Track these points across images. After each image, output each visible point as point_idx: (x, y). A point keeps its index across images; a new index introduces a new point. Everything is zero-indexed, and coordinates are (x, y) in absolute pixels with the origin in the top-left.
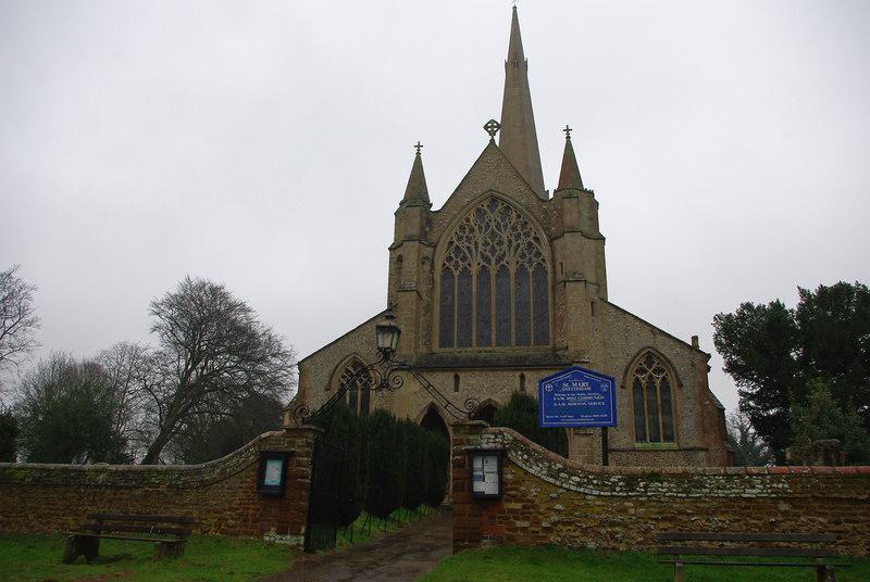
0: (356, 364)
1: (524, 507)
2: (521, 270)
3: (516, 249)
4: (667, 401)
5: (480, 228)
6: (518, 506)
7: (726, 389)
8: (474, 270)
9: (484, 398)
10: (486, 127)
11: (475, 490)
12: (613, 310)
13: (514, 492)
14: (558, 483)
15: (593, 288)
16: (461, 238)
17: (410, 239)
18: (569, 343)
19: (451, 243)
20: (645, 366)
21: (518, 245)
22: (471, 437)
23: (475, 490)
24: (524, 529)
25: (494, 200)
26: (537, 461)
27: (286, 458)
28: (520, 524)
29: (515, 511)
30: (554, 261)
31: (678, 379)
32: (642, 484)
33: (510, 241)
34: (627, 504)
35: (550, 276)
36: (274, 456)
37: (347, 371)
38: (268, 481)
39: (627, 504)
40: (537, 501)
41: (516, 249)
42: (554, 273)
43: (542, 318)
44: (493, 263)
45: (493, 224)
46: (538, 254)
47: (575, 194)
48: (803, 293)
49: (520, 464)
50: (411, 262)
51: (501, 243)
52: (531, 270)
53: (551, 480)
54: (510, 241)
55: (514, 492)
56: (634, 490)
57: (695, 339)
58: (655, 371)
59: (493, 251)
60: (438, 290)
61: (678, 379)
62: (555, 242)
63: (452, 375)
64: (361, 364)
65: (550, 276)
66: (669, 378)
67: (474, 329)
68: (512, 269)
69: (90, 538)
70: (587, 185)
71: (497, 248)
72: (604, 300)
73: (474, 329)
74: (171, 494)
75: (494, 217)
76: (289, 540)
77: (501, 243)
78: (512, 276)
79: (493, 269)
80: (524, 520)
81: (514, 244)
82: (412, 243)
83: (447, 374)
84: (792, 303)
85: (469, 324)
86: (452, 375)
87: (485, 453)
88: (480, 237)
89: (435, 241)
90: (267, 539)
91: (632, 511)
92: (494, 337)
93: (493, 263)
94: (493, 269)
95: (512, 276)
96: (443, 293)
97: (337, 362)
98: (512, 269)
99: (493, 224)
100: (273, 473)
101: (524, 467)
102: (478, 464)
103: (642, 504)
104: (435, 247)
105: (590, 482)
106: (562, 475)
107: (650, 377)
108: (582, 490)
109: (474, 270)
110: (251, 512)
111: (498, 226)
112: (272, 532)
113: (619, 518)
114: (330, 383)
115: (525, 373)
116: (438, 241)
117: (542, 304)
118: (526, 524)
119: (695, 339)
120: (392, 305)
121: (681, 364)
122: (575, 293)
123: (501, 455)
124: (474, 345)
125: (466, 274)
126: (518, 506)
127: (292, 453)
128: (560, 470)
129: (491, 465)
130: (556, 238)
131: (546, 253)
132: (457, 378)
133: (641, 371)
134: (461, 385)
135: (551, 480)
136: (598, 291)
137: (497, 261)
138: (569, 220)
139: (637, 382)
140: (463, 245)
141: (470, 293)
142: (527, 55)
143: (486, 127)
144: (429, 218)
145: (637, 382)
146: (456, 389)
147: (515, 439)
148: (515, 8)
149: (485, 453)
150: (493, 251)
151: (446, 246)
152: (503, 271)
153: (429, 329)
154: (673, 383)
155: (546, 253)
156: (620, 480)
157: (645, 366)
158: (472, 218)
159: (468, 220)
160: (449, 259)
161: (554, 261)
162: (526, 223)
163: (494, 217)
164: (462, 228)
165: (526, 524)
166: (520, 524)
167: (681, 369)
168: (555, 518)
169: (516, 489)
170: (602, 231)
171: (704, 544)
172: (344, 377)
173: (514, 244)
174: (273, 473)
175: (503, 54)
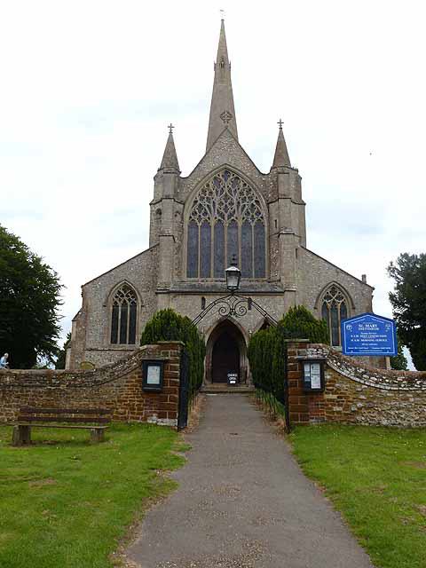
0: (126, 288)
1: (338, 397)
2: (246, 224)
3: (243, 209)
5: (217, 192)
6: (335, 397)
8: (213, 222)
11: (158, 383)
12: (309, 255)
13: (331, 388)
14: (362, 382)
15: (297, 239)
16: (202, 199)
17: (168, 198)
18: (282, 277)
19: (196, 202)
20: (330, 294)
22: (300, 350)
23: (158, 383)
24: (339, 412)
25: (227, 172)
26: (347, 367)
27: (162, 364)
28: (336, 409)
29: (333, 400)
30: (269, 218)
31: (353, 304)
32: (418, 382)
33: (239, 203)
34: (408, 395)
36: (154, 363)
37: (119, 292)
39: (408, 395)
40: (348, 393)
41: (243, 209)
42: (269, 226)
43: (260, 259)
44: (226, 218)
45: (226, 190)
47: (286, 170)
49: (335, 368)
50: (168, 215)
51: (232, 204)
52: (253, 224)
53: (358, 380)
54: (239, 203)
55: (331, 388)
56: (412, 386)
57: (364, 276)
59: (226, 209)
60: (186, 236)
61: (353, 304)
64: (130, 288)
65: (266, 229)
66: (346, 302)
67: (212, 265)
68: (240, 223)
69: (27, 426)
70: (294, 164)
73: (212, 265)
74: (69, 391)
75: (227, 184)
76: (167, 422)
77: (232, 204)
78: (240, 228)
79: (226, 223)
80: (339, 405)
81: (242, 204)
82: (168, 200)
86: (198, 299)
87: (311, 362)
88: (217, 199)
90: (151, 422)
91: (412, 400)
93: (226, 218)
94: (226, 223)
95: (240, 228)
96: (190, 238)
97: (112, 286)
98: (240, 223)
99: (226, 190)
100: (154, 376)
101: (338, 370)
102: (307, 368)
103: (418, 395)
105: (383, 381)
106: (365, 376)
108: (378, 386)
109: (213, 222)
110: (137, 403)
111: (230, 191)
112: (155, 417)
113: (403, 405)
114: (107, 300)
115: (253, 298)
116: (187, 199)
117: (260, 248)
118: (340, 409)
119: (364, 276)
120: (154, 247)
122: (287, 243)
123: (322, 363)
124: (212, 276)
125: (206, 225)
126: (335, 397)
127: (167, 361)
128: (363, 373)
129: (316, 369)
130: (271, 203)
133: (328, 297)
135: (358, 380)
136: (300, 242)
137: (229, 217)
138: (282, 190)
141: (209, 238)
142: (230, 58)
144: (181, 182)
147: (331, 352)
149: (311, 362)
150: (226, 209)
151: (192, 203)
152: (233, 224)
153: (180, 263)
154: (349, 307)
155: (264, 213)
156: (404, 380)
157: (330, 294)
158: (210, 184)
159: (208, 185)
161: (269, 218)
162: (250, 190)
163: (227, 184)
164: (204, 192)
165: (340, 409)
166: (336, 409)
167: (355, 297)
168: (360, 405)
169: (333, 386)
170: (304, 198)
171: (84, 416)
172: (116, 297)
173: (242, 204)
174: (154, 376)
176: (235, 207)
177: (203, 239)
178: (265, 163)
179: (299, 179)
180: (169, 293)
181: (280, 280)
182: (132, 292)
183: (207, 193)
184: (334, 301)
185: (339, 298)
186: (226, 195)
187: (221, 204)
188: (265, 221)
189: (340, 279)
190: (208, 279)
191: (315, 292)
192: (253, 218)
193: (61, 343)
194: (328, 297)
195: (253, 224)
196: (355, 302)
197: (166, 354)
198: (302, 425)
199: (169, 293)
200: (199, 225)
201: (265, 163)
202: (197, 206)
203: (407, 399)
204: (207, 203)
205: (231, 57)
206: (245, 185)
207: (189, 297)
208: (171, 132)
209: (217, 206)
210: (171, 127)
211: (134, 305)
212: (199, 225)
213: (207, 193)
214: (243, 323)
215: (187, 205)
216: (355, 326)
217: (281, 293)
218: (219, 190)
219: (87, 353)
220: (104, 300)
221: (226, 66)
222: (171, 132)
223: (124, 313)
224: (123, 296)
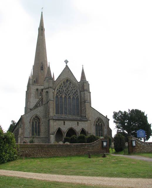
0: (37, 117)
3: (72, 93)
4: (101, 128)
5: (64, 86)
6: (137, 147)
7: (113, 126)
8: (63, 96)
9: (70, 127)
10: (65, 61)
19: (58, 89)
21: (73, 92)
25: (67, 80)
28: (138, 149)
33: (71, 91)
35: (79, 100)
37: (34, 118)
38: (104, 145)
41: (72, 93)
44: (67, 95)
46: (77, 94)
48: (129, 110)
51: (69, 91)
58: (100, 122)
59: (67, 92)
62: (81, 92)
63: (63, 121)
65: (79, 100)
71: (68, 92)
72: (91, 106)
77: (69, 91)
78: (71, 99)
82: (51, 89)
83: (62, 121)
84: (127, 111)
85: (62, 109)
86: (63, 121)
87: (133, 141)
89: (54, 88)
92: (68, 113)
95: (71, 99)
100: (105, 144)
104: (55, 90)
107: (99, 123)
109: (63, 96)
119: (107, 116)
121: (104, 121)
125: (61, 97)
126: (137, 147)
129: (134, 142)
131: (79, 94)
132: (64, 122)
133: (97, 122)
134: (65, 124)
137: (68, 95)
139: (96, 124)
140: (61, 90)
141: (62, 102)
143: (65, 61)
145: (96, 124)
146: (64, 125)
148: (42, 12)
149: (133, 141)
150: (67, 92)
155: (79, 94)
159: (61, 84)
160: (57, 93)
162: (74, 87)
167: (104, 122)
168: (141, 148)
175: (38, 26)
176: (70, 92)
177: (60, 102)
178: (78, 79)
179: (89, 85)
180: (54, 119)
181: (85, 116)
182: (39, 118)
183: (61, 86)
184: (99, 123)
185: (100, 122)
186: (67, 88)
187: (66, 91)
188: (79, 97)
189: (100, 116)
190: (63, 115)
191: (94, 120)
192: (59, 95)
193: (146, 141)
194: (97, 122)
195: (75, 98)
196: (105, 123)
197: (107, 140)
198: (108, 154)
199: (54, 119)
200: (59, 97)
201: (78, 79)
202: (58, 91)
203: (149, 147)
204: (61, 90)
205: (45, 26)
206: (73, 85)
207: (60, 121)
208: (83, 68)
209: (64, 91)
210: (66, 62)
211: (39, 123)
212: (59, 97)
213: (61, 86)
214: (76, 130)
215: (55, 90)
216: (139, 132)
217: (87, 121)
218: (65, 86)
219: (24, 138)
220: (29, 121)
221: (43, 30)
222: (83, 68)
223: (36, 125)
224: (35, 120)
